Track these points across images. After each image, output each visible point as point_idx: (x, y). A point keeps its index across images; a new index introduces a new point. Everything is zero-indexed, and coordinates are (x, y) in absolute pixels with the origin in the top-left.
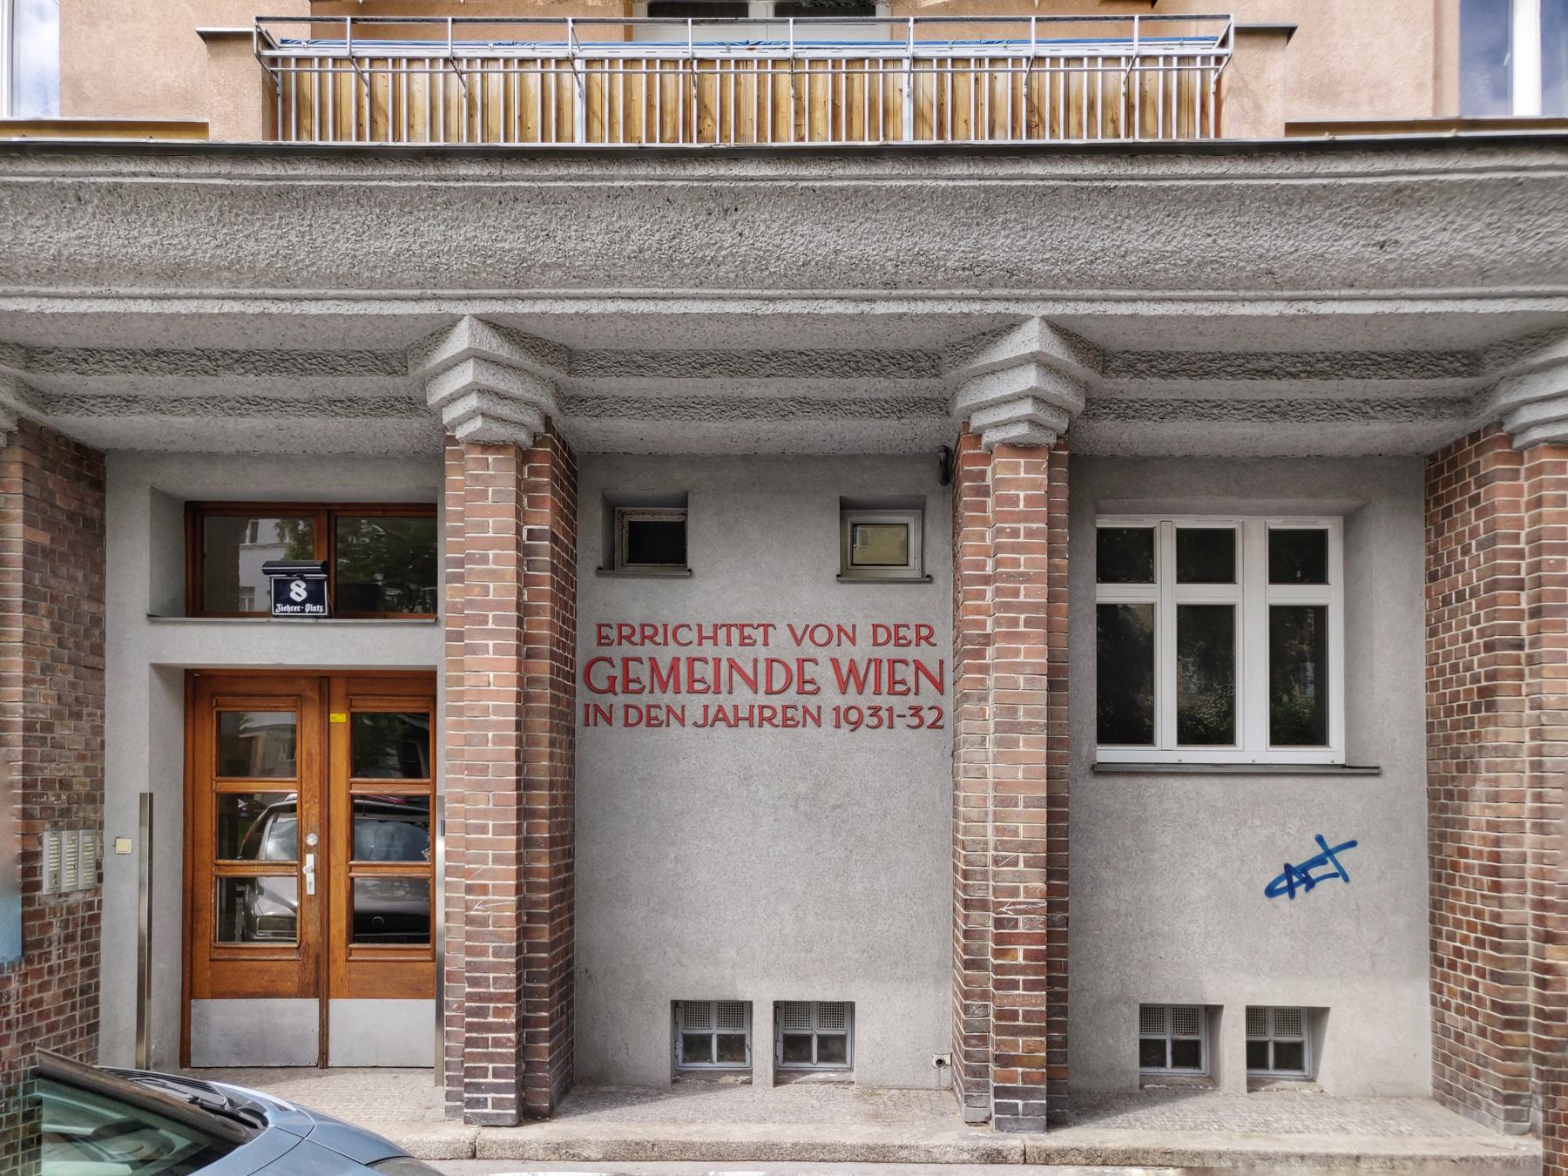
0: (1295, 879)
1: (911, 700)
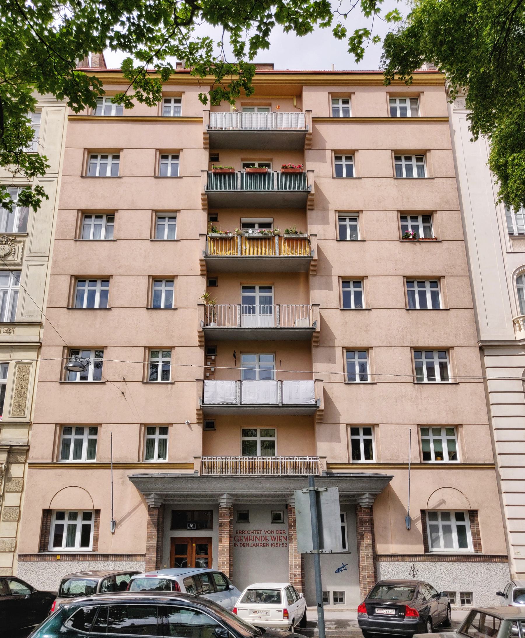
0: (339, 570)
1: (282, 542)
